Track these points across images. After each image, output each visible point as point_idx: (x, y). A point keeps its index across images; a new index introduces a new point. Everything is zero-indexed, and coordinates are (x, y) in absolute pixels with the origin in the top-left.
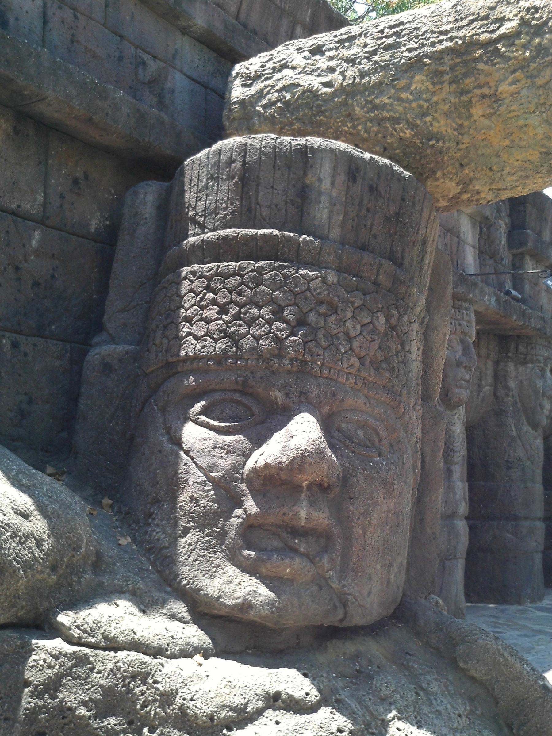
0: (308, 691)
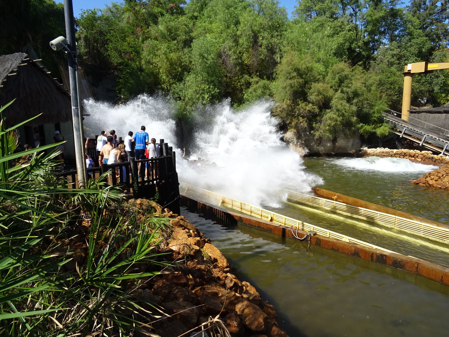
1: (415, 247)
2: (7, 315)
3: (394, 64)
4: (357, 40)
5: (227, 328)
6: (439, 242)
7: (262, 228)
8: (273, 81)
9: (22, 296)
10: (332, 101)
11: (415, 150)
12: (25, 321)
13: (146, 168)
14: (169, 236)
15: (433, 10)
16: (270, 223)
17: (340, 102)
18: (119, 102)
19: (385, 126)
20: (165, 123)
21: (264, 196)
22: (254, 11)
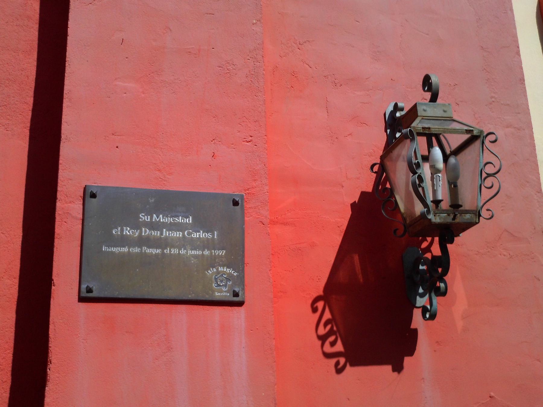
13: (149, 251)
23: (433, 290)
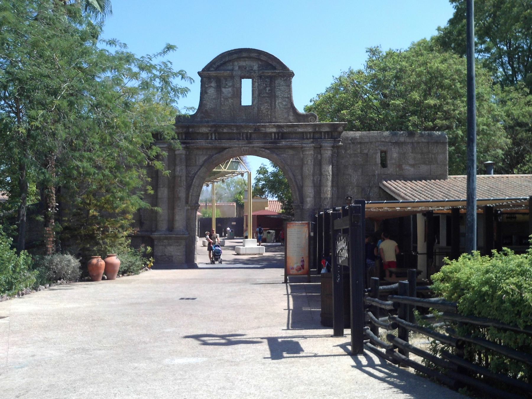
0: (264, 348)
1: (471, 196)
2: (75, 287)
3: (109, 237)
4: (372, 393)
5: (413, 297)
6: (292, 338)
7: (302, 175)
8: (374, 49)
9: (350, 233)
10: (36, 202)
11: (522, 255)
12: (306, 276)
14: (44, 341)
15: (393, 118)
16: (234, 232)
17: (234, 387)
18: (364, 314)
19: (92, 317)
20: (484, 271)
21: (21, 296)
22: (46, 267)
23: (337, 144)
